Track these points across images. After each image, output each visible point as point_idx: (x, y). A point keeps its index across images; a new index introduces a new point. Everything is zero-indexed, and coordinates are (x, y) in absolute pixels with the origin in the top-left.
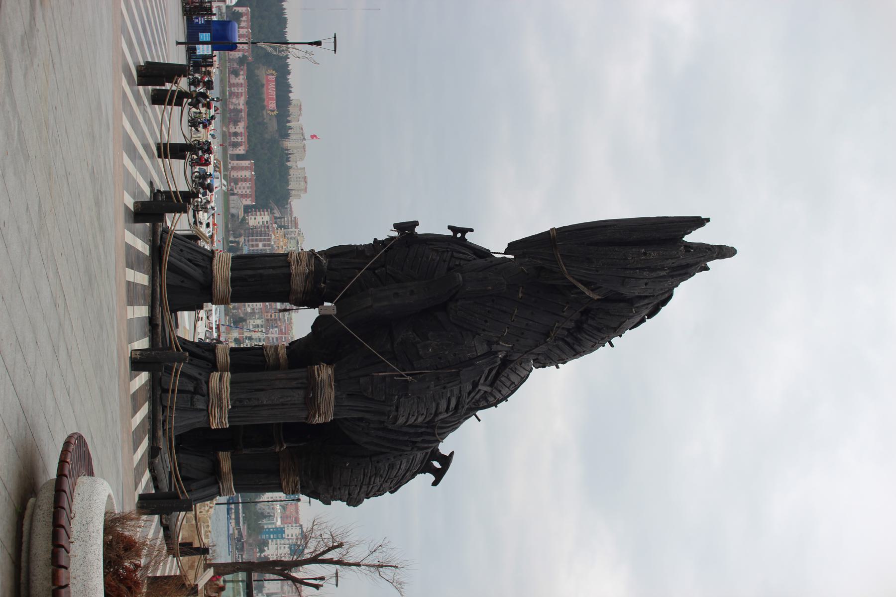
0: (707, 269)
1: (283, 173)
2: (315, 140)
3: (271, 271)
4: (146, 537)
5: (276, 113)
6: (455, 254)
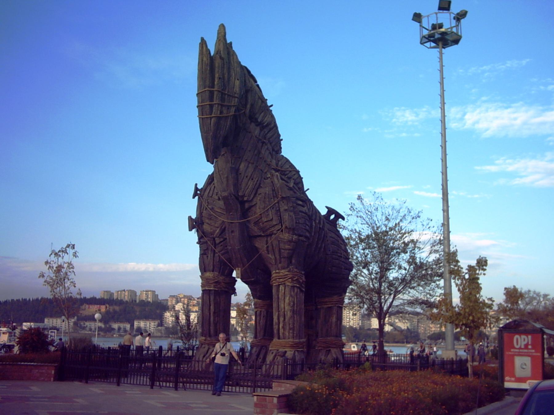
0: (231, 43)
1: (144, 304)
2: (75, 247)
3: (212, 307)
4: (290, 241)
5: (108, 306)
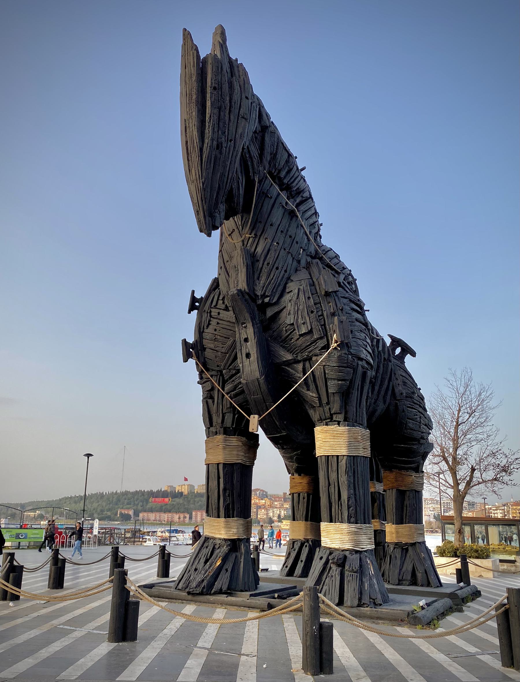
3: (221, 480)
5: (170, 498)
6: (212, 306)
